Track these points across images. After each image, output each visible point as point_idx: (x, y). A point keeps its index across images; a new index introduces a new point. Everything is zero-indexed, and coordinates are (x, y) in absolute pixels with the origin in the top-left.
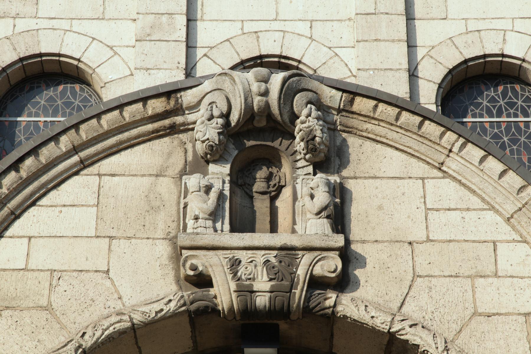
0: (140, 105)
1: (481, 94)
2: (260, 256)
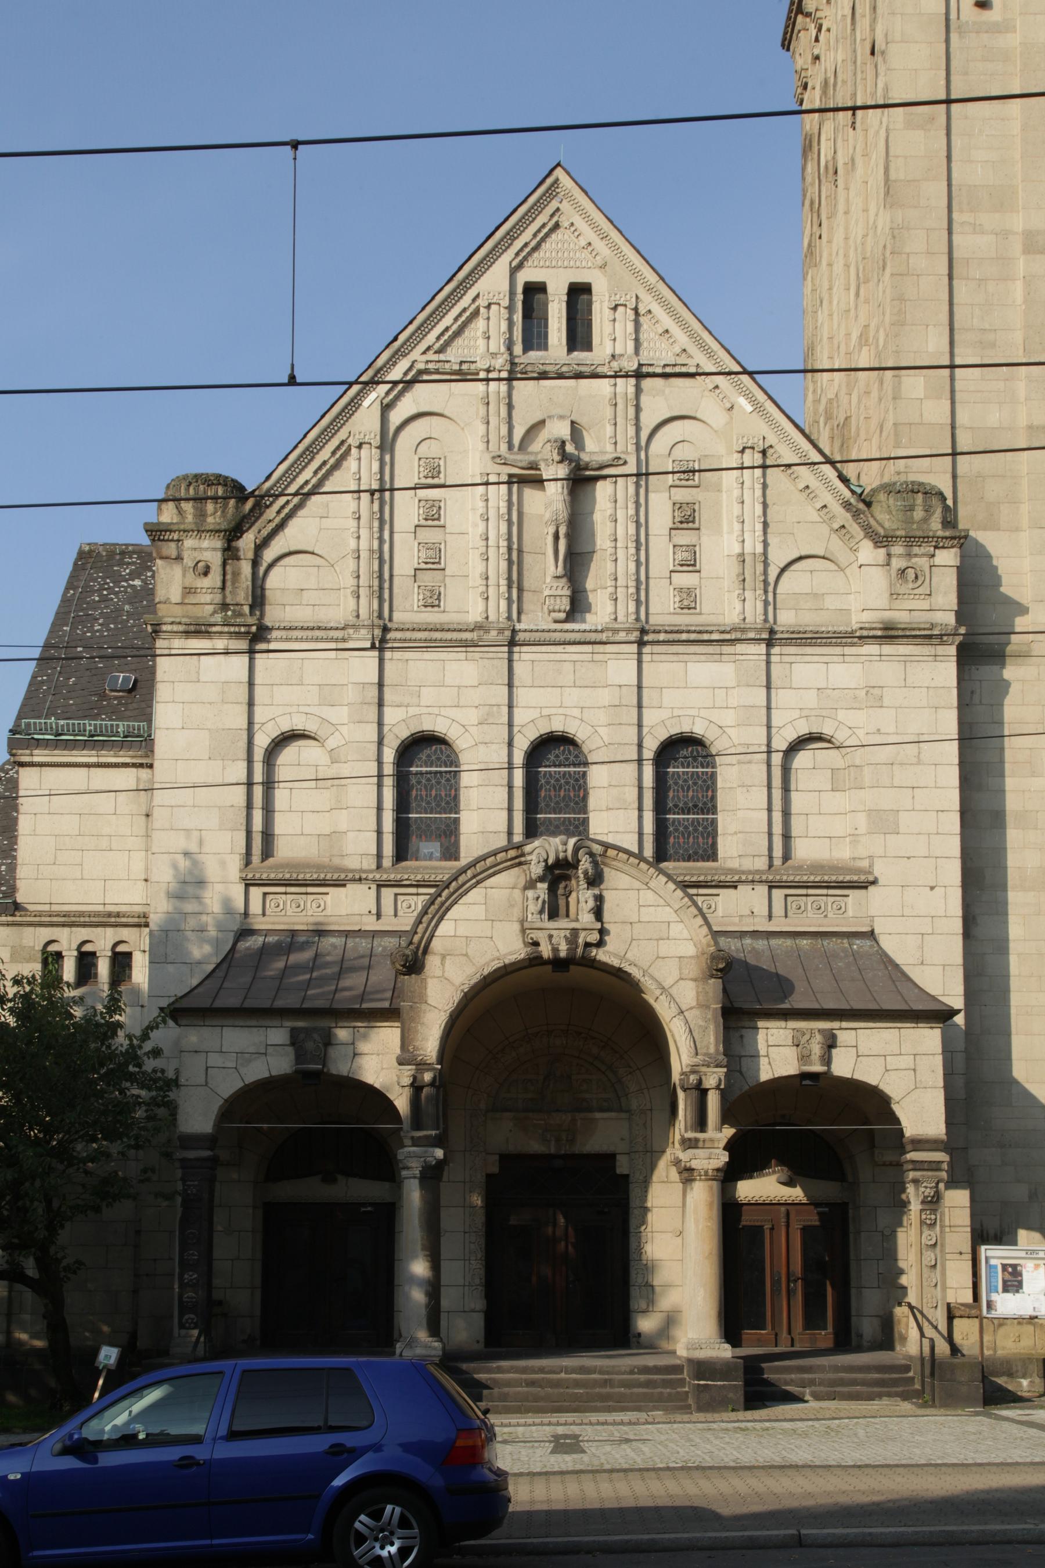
1: (550, 752)
2: (562, 933)
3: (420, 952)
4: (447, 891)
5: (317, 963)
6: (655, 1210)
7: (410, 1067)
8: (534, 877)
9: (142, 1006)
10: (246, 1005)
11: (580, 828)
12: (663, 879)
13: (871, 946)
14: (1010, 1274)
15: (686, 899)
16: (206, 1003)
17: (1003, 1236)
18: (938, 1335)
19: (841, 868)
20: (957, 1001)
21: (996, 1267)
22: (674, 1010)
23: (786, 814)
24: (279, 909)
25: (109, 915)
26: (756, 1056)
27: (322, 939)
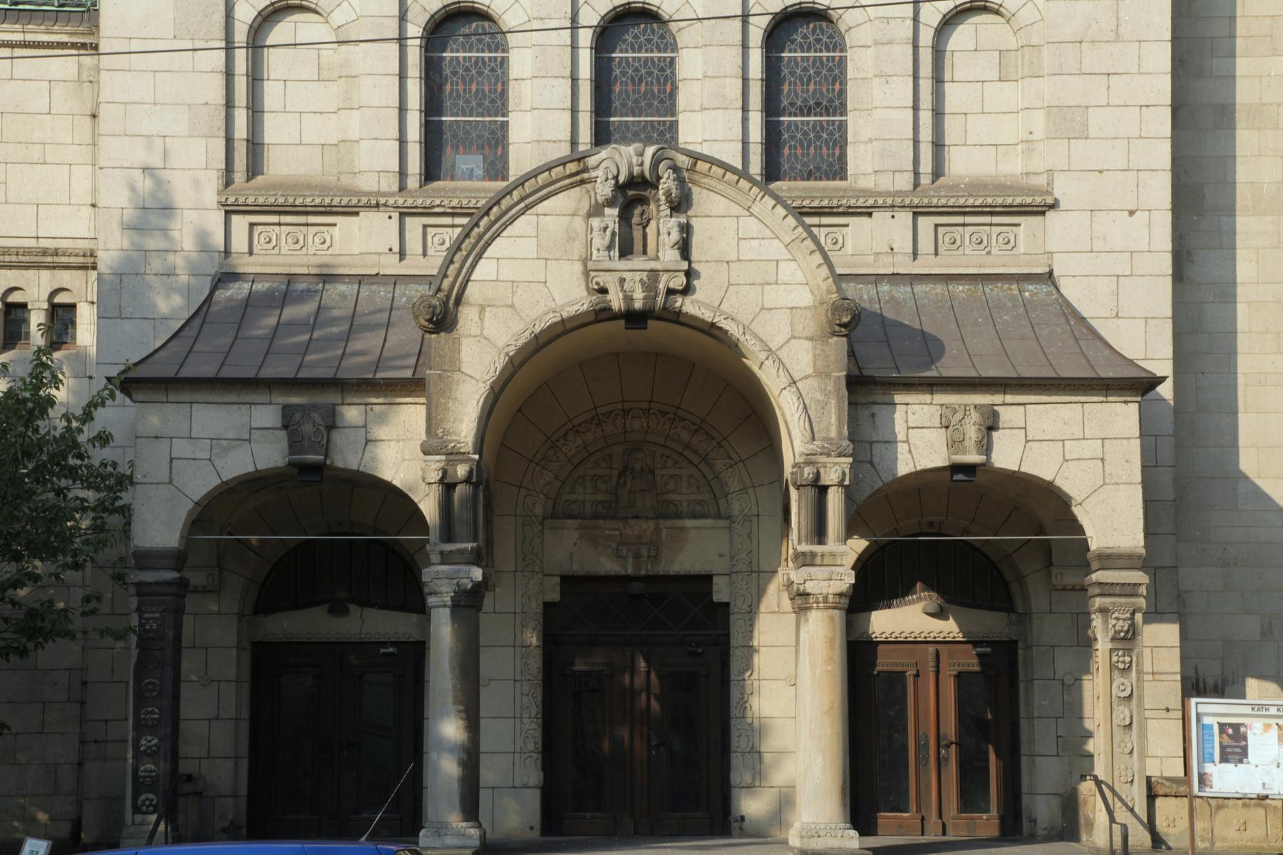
0: (561, 168)
1: (627, 32)
2: (638, 276)
3: (452, 302)
4: (486, 218)
5: (321, 318)
6: (762, 650)
7: (438, 457)
8: (600, 200)
9: (90, 378)
10: (223, 374)
11: (667, 134)
12: (770, 202)
13: (1049, 294)
14: (1230, 737)
15: (800, 229)
16: (169, 372)
17: (1224, 687)
18: (1135, 821)
19: (1011, 187)
20: (1163, 367)
21: (1211, 727)
22: (784, 380)
23: (938, 113)
24: (270, 246)
25: (45, 252)
26: (893, 442)
27: (327, 286)
